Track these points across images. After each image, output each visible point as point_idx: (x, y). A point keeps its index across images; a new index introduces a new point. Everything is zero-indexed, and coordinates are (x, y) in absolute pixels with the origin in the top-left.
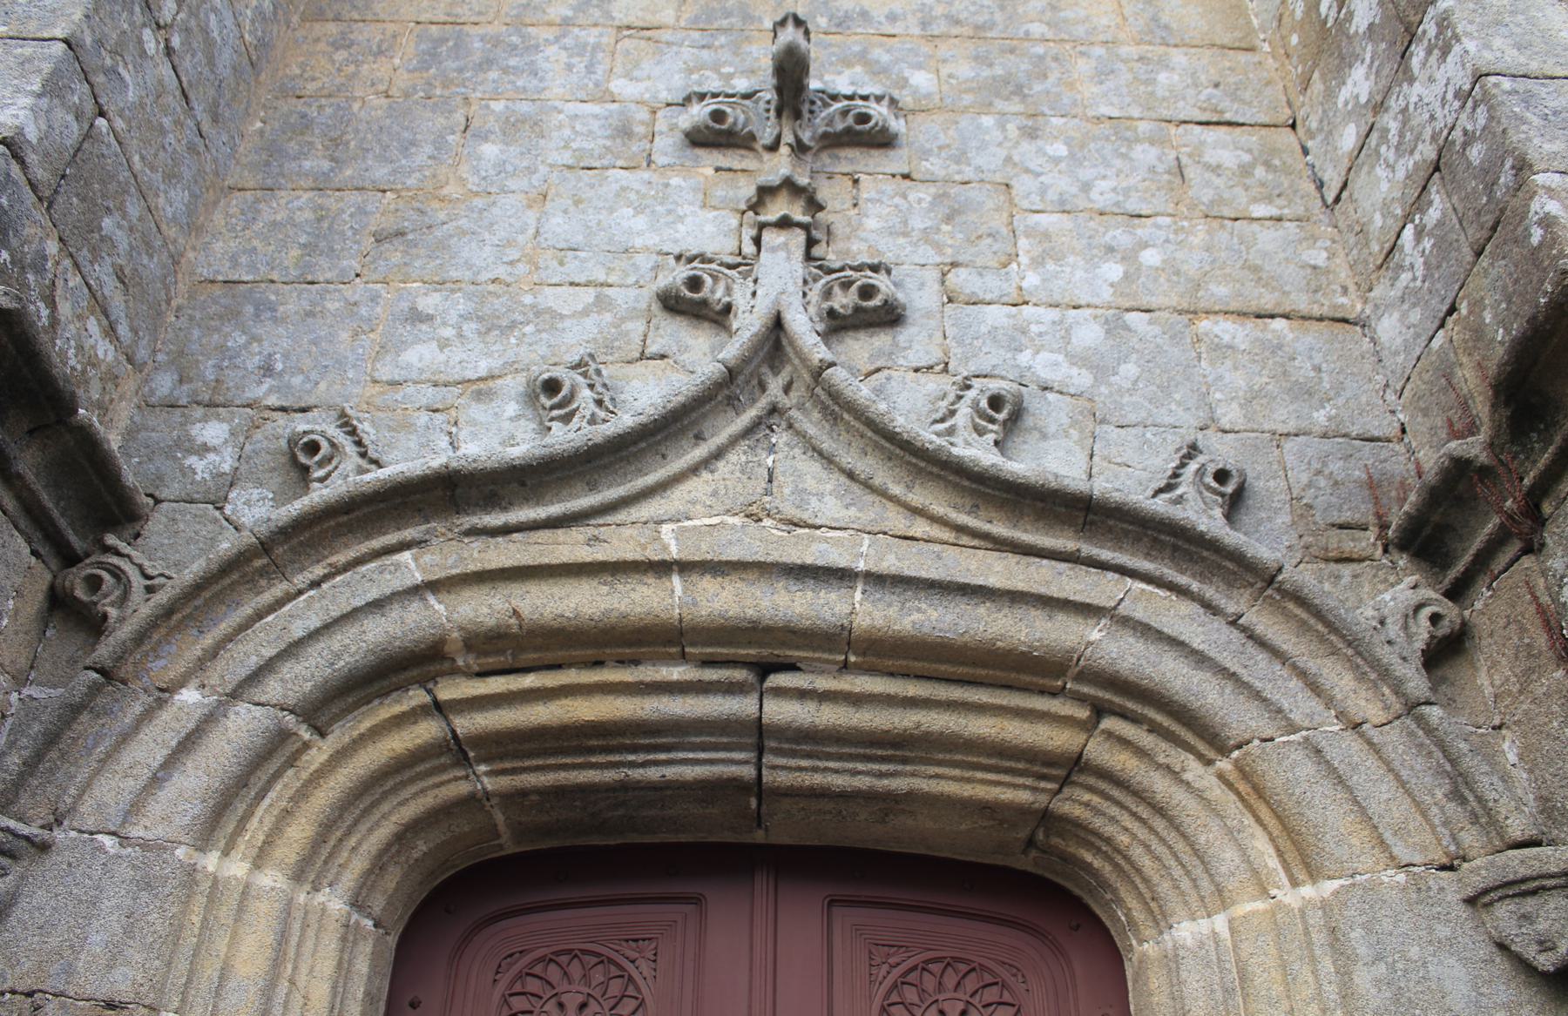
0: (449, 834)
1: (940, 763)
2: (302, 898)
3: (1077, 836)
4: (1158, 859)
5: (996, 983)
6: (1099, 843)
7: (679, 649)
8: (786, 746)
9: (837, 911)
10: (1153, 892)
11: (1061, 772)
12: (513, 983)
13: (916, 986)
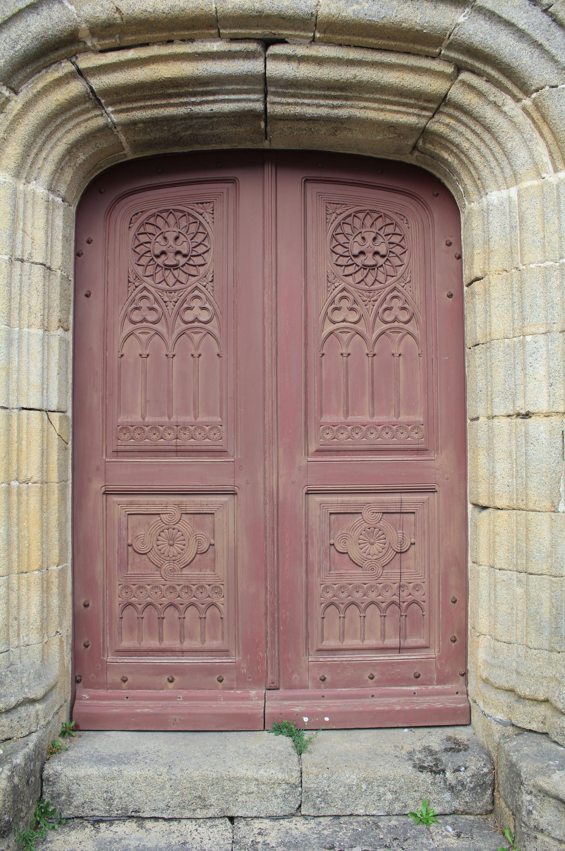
0: (96, 149)
1: (367, 100)
2: (21, 187)
3: (441, 144)
4: (484, 156)
5: (392, 224)
6: (452, 148)
7: (216, 31)
8: (280, 90)
9: (309, 185)
10: (479, 175)
11: (434, 106)
12: (139, 228)
13: (350, 225)
